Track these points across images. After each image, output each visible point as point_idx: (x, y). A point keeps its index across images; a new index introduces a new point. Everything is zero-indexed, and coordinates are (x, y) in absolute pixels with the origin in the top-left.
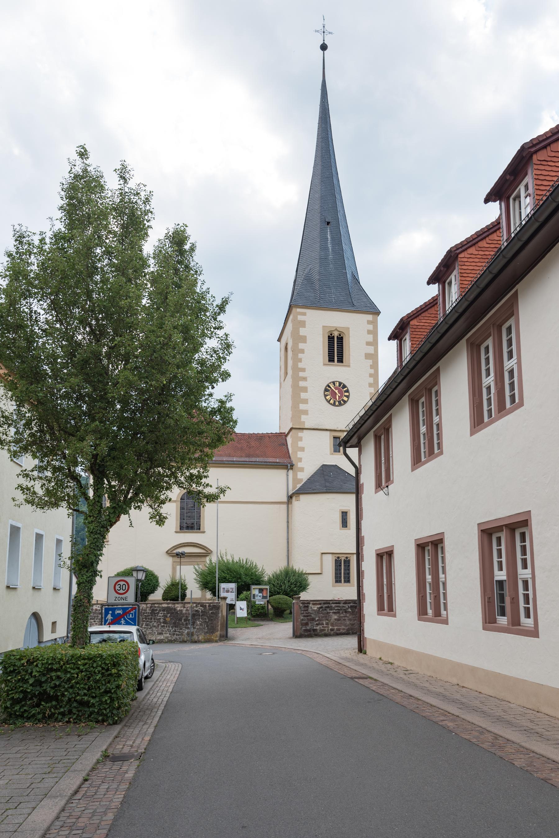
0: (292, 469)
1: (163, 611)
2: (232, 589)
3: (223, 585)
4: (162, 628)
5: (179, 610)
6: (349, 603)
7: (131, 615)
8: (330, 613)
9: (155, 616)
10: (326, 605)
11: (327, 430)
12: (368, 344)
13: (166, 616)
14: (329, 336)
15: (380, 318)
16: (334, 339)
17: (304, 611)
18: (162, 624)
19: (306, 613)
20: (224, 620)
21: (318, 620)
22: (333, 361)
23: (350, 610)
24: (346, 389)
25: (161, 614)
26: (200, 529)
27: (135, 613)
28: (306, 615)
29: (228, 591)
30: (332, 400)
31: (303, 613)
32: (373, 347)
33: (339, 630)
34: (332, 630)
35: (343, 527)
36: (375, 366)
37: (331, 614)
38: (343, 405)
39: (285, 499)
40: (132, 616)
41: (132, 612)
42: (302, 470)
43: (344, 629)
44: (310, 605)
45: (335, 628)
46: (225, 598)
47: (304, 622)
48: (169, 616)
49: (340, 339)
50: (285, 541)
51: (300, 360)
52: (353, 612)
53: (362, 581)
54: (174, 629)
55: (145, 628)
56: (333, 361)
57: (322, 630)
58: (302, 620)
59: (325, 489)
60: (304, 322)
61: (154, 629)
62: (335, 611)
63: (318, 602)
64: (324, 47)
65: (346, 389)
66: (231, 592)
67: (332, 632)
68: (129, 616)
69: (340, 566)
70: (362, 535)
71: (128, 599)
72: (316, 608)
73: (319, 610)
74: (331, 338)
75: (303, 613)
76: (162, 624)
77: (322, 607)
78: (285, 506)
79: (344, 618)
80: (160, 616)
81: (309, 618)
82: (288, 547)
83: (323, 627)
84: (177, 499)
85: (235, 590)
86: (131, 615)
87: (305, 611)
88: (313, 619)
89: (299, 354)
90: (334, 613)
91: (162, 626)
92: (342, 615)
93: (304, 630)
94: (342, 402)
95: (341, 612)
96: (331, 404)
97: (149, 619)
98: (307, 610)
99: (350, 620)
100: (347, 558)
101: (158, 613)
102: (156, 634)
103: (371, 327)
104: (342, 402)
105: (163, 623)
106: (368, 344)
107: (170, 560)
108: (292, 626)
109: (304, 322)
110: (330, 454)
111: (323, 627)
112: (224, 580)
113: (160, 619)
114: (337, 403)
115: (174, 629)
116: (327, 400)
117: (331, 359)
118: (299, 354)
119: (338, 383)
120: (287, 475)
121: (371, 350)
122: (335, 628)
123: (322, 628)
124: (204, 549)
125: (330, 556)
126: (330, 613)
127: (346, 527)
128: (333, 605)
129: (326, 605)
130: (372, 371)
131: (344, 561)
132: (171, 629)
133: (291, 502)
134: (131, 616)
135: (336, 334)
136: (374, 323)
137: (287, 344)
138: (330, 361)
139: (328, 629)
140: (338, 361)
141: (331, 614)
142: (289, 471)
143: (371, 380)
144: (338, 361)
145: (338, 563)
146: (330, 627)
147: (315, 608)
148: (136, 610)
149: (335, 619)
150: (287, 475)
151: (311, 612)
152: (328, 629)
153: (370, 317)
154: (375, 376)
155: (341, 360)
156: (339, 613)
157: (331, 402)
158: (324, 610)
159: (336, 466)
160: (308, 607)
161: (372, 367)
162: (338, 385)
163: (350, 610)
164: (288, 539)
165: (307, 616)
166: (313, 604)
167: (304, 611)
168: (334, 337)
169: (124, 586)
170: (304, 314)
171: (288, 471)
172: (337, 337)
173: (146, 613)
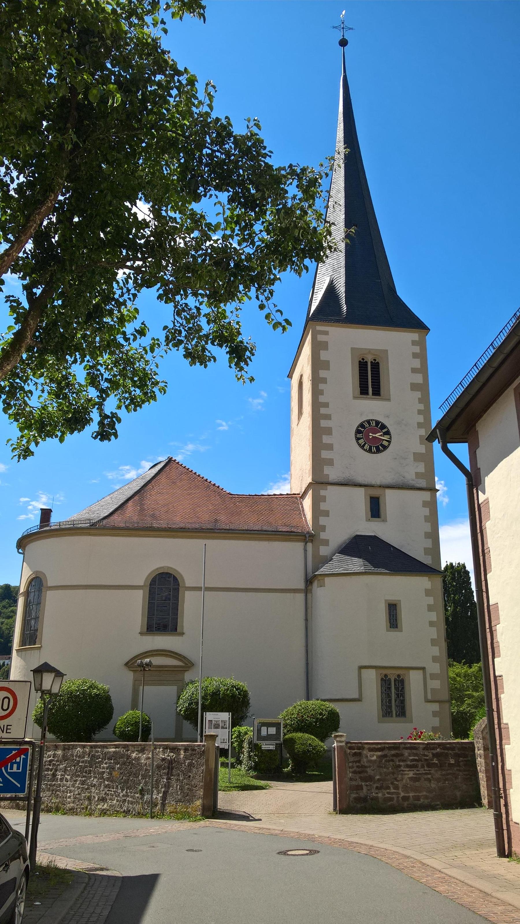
0: (312, 541)
1: (108, 759)
2: (224, 722)
3: (210, 716)
4: (106, 789)
5: (135, 758)
6: (433, 749)
7: (15, 766)
8: (400, 766)
9: (96, 767)
10: (393, 752)
11: (361, 485)
12: (414, 371)
13: (114, 769)
14: (360, 362)
15: (429, 338)
16: (367, 365)
17: (353, 762)
18: (107, 783)
19: (357, 767)
20: (211, 778)
21: (379, 780)
22: (367, 393)
23: (435, 761)
24: (385, 430)
25: (106, 764)
26: (176, 629)
27: (25, 761)
28: (358, 769)
29: (217, 726)
30: (367, 445)
31: (352, 767)
32: (421, 375)
33: (417, 798)
34: (405, 798)
35: (391, 627)
36: (425, 400)
37: (402, 768)
38: (382, 451)
39: (301, 585)
40: (18, 768)
41: (18, 760)
42: (326, 543)
43: (426, 797)
44: (365, 752)
45: (411, 795)
46: (213, 737)
47: (354, 783)
48: (118, 768)
49: (376, 366)
50: (303, 649)
51: (322, 393)
52: (441, 766)
53: (498, 699)
54: (124, 792)
55: (79, 788)
56: (367, 393)
57: (386, 800)
58: (351, 779)
59: (363, 568)
60: (327, 343)
61: (93, 790)
62: (409, 763)
63: (379, 746)
64: (343, 43)
65: (385, 430)
66: (223, 728)
67: (406, 804)
68: (12, 768)
69: (390, 688)
70: (491, 602)
71: (13, 729)
72: (375, 758)
73: (381, 761)
74: (362, 365)
75: (352, 767)
76: (107, 783)
77: (385, 756)
78: (301, 597)
79: (426, 777)
80: (103, 768)
81: (362, 775)
82: (307, 659)
83: (388, 793)
84: (145, 583)
85: (229, 723)
86: (15, 766)
87: (356, 762)
88: (370, 779)
89: (320, 385)
90: (408, 766)
91: (106, 786)
92: (422, 771)
93: (355, 798)
94: (380, 447)
95: (420, 764)
96: (365, 450)
97: (86, 773)
98: (359, 761)
99: (438, 780)
100: (399, 676)
101: (101, 762)
102: (96, 799)
103: (417, 349)
104: (380, 447)
105: (108, 779)
106: (414, 371)
107: (129, 676)
108: (332, 788)
109: (327, 343)
110: (366, 521)
111: (388, 793)
112: (212, 708)
113: (104, 772)
114: (374, 449)
115: (124, 792)
116: (359, 445)
117: (364, 391)
118: (320, 385)
119: (374, 422)
120: (305, 550)
121: (418, 379)
122: (411, 795)
123: (387, 795)
124: (180, 660)
125: (373, 672)
126: (400, 766)
127: (397, 627)
128: (406, 753)
129: (393, 752)
130: (422, 407)
131: (395, 680)
132: (120, 791)
133: (311, 590)
134: (15, 769)
135: (369, 359)
136: (422, 344)
137: (301, 376)
138: (362, 393)
139: (398, 797)
140: (374, 394)
141: (402, 768)
142: (308, 544)
143: (421, 419)
144: (374, 394)
145: (385, 682)
146: (402, 794)
147: (374, 757)
148: (27, 756)
149: (411, 779)
150: (305, 550)
151: (366, 764)
152: (398, 797)
153: (413, 336)
154: (426, 412)
155: (377, 392)
156: (415, 766)
157: (365, 448)
158: (389, 761)
159: (375, 538)
160: (360, 754)
161: (420, 401)
162: (374, 425)
163: (435, 761)
164: (307, 646)
165: (360, 773)
166: (371, 750)
167: (353, 762)
168: (366, 362)
169: (6, 700)
170: (326, 333)
171: (306, 544)
172: (371, 362)
173: (83, 762)
